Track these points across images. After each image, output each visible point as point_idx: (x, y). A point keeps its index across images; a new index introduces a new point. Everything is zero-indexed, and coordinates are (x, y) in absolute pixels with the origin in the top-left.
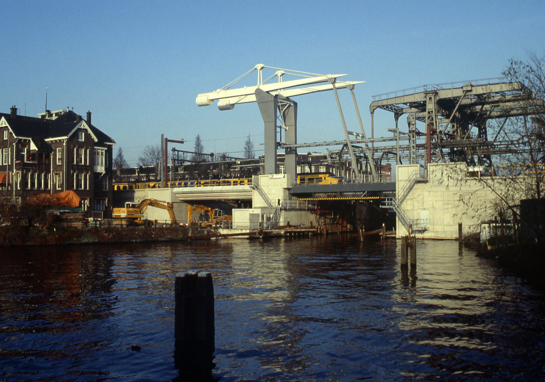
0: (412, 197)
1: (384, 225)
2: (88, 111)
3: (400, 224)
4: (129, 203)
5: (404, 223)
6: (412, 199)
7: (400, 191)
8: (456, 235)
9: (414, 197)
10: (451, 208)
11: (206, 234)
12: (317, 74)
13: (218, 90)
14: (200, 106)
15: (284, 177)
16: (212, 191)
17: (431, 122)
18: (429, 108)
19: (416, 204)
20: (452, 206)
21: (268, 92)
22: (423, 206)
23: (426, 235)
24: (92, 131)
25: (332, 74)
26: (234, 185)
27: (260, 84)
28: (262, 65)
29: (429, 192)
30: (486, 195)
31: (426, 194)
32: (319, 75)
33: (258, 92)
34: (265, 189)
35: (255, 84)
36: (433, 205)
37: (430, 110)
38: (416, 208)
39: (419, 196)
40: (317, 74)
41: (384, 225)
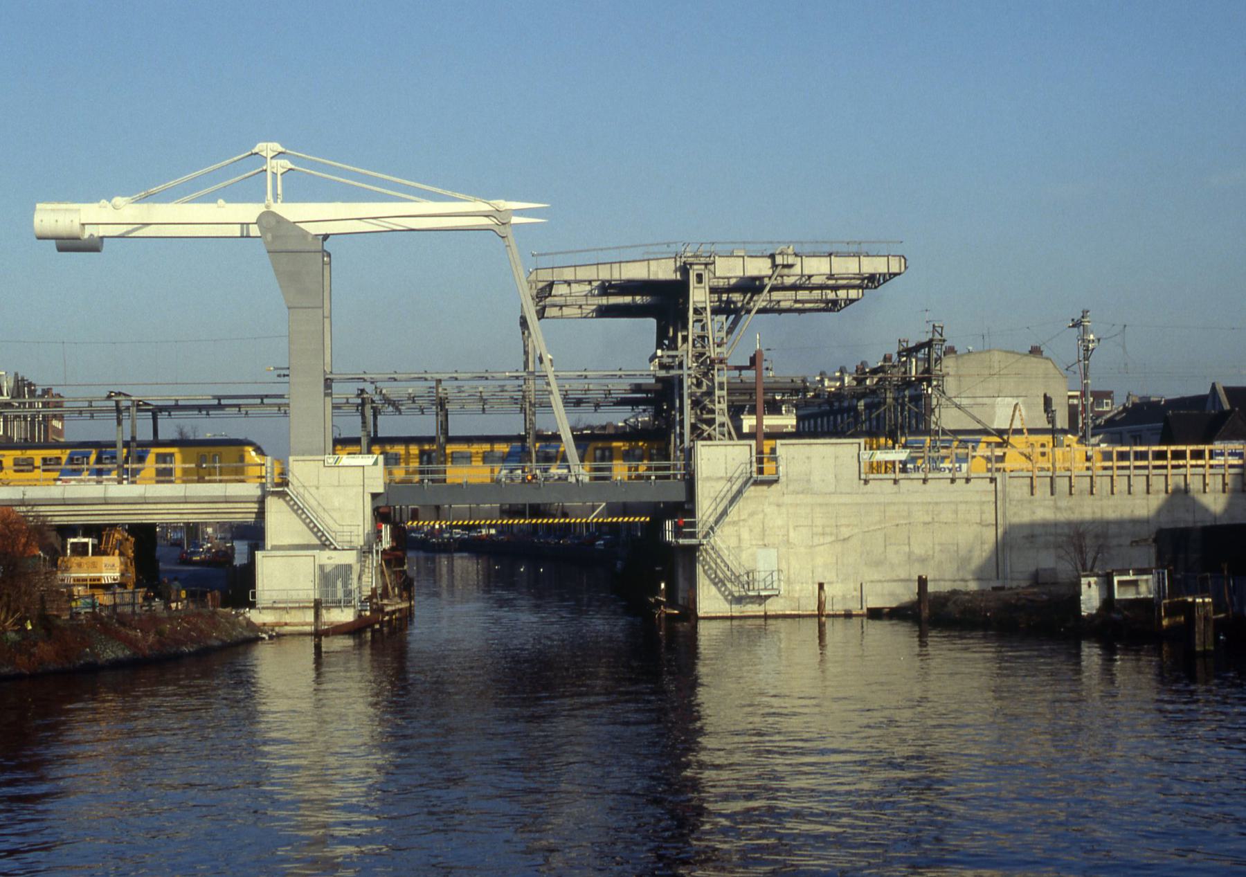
0: (736, 519)
1: (663, 586)
2: (952, 337)
3: (707, 582)
4: (85, 540)
5: (718, 582)
6: (734, 523)
7: (705, 508)
8: (812, 608)
9: (742, 518)
10: (830, 543)
11: (1210, 600)
12: (449, 193)
13: (118, 200)
14: (39, 238)
15: (376, 463)
16: (105, 498)
17: (701, 333)
18: (695, 299)
19: (745, 535)
20: (833, 538)
21: (295, 223)
22: (763, 540)
23: (773, 607)
24: (1228, 399)
25: (506, 200)
26: (185, 482)
27: (275, 201)
28: (278, 147)
29: (778, 506)
30: (910, 513)
31: (769, 510)
32: (458, 195)
33: (270, 222)
34: (310, 499)
35: (259, 197)
36: (788, 535)
37: (699, 305)
38: (745, 544)
39: (752, 514)
40: (449, 193)
41: (663, 586)
